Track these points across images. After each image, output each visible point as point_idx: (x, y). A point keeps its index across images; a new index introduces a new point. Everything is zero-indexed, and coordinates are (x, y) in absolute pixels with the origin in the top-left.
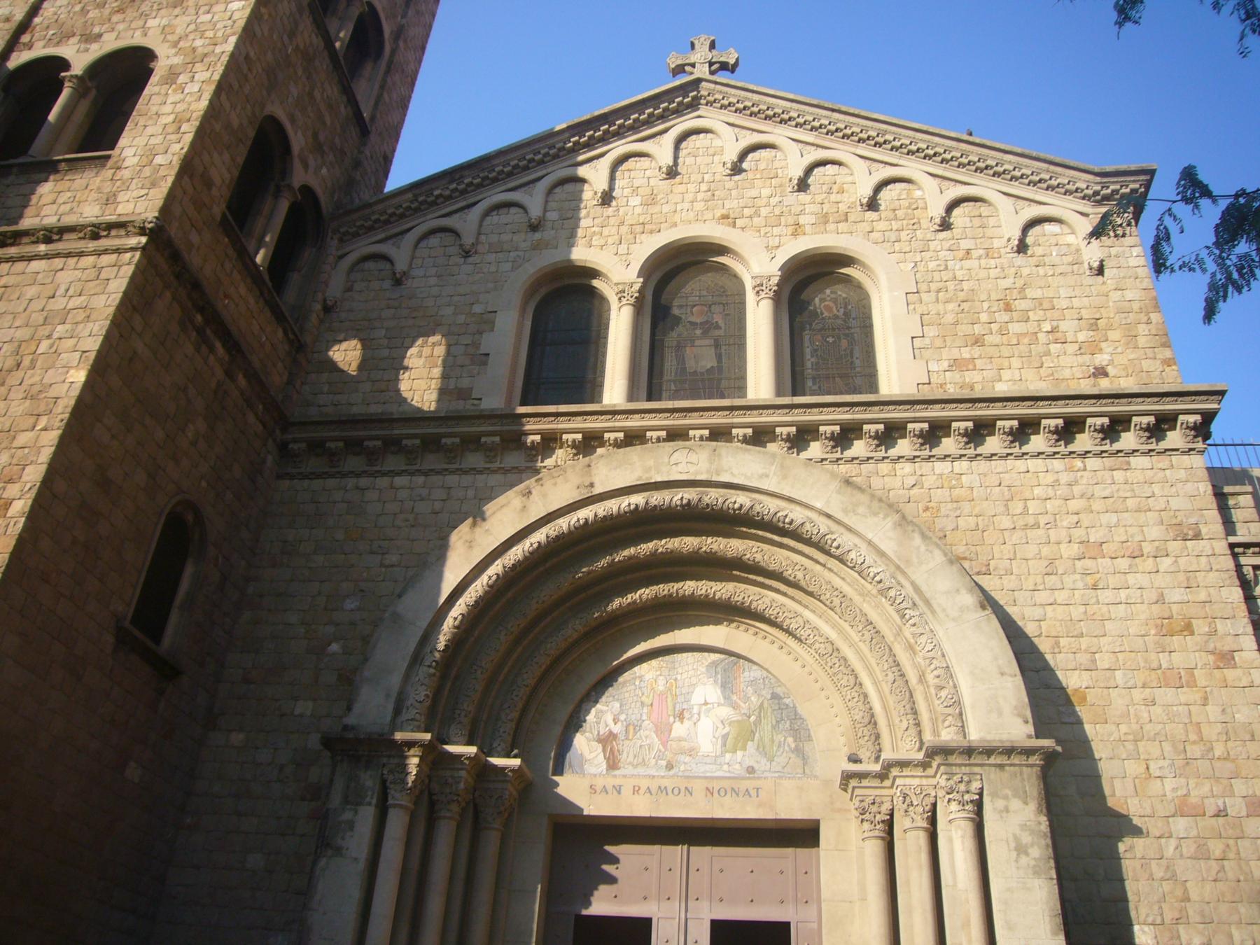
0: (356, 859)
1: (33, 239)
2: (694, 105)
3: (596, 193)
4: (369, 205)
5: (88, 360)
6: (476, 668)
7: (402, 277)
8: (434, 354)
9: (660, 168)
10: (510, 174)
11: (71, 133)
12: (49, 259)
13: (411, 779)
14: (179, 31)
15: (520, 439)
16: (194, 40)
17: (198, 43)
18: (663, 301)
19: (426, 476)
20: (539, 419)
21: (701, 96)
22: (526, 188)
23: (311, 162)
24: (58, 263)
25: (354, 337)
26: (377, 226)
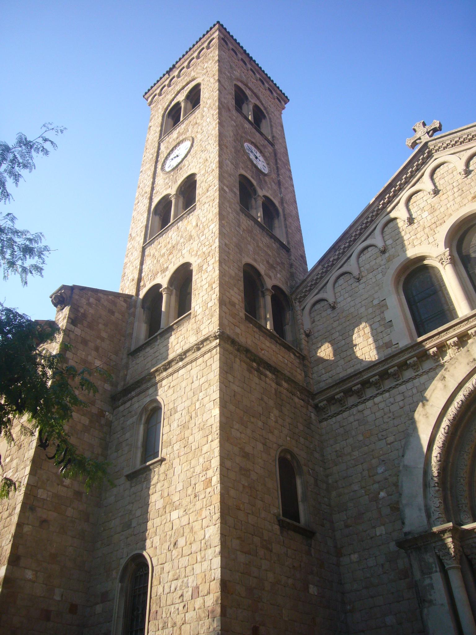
0: (442, 604)
1: (176, 362)
2: (430, 155)
3: (404, 221)
4: (305, 280)
5: (217, 403)
6: (459, 478)
7: (334, 305)
8: (366, 333)
9: (429, 193)
10: (360, 234)
11: (173, 312)
12: (185, 367)
13: (452, 551)
14: (195, 249)
15: (427, 354)
16: (202, 249)
17: (204, 249)
18: (464, 254)
19: (389, 392)
20: (431, 340)
21: (431, 150)
22: (371, 236)
23: (271, 274)
24: (189, 367)
25: (326, 342)
26: (312, 288)
